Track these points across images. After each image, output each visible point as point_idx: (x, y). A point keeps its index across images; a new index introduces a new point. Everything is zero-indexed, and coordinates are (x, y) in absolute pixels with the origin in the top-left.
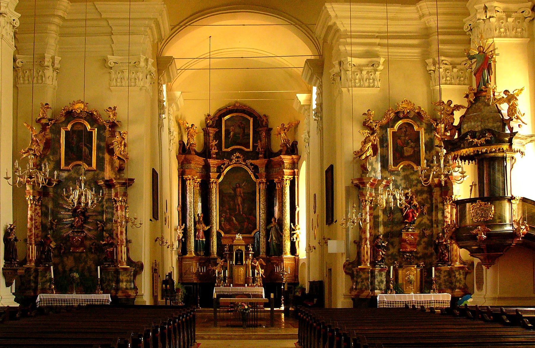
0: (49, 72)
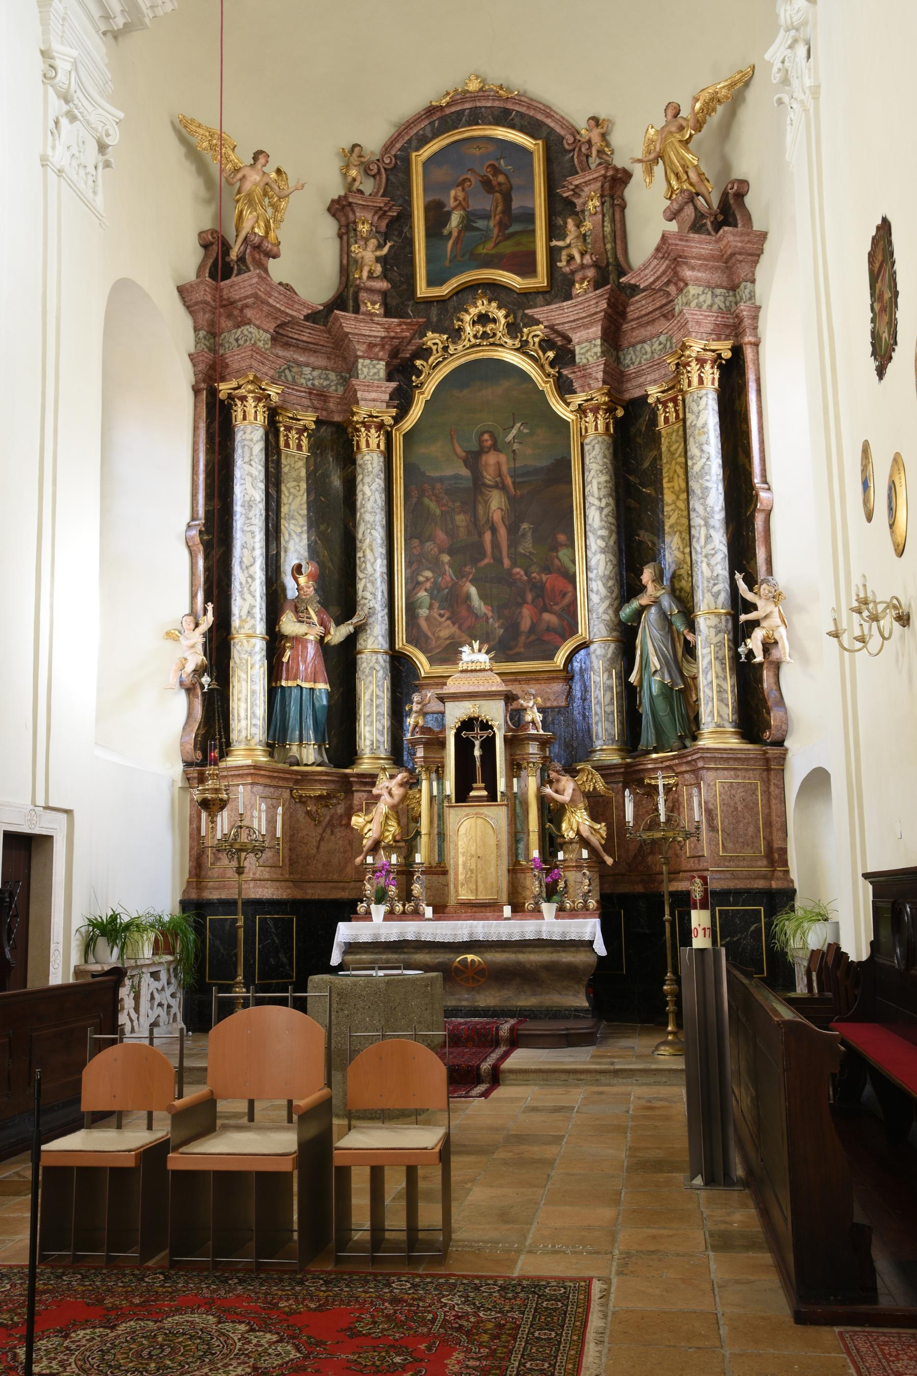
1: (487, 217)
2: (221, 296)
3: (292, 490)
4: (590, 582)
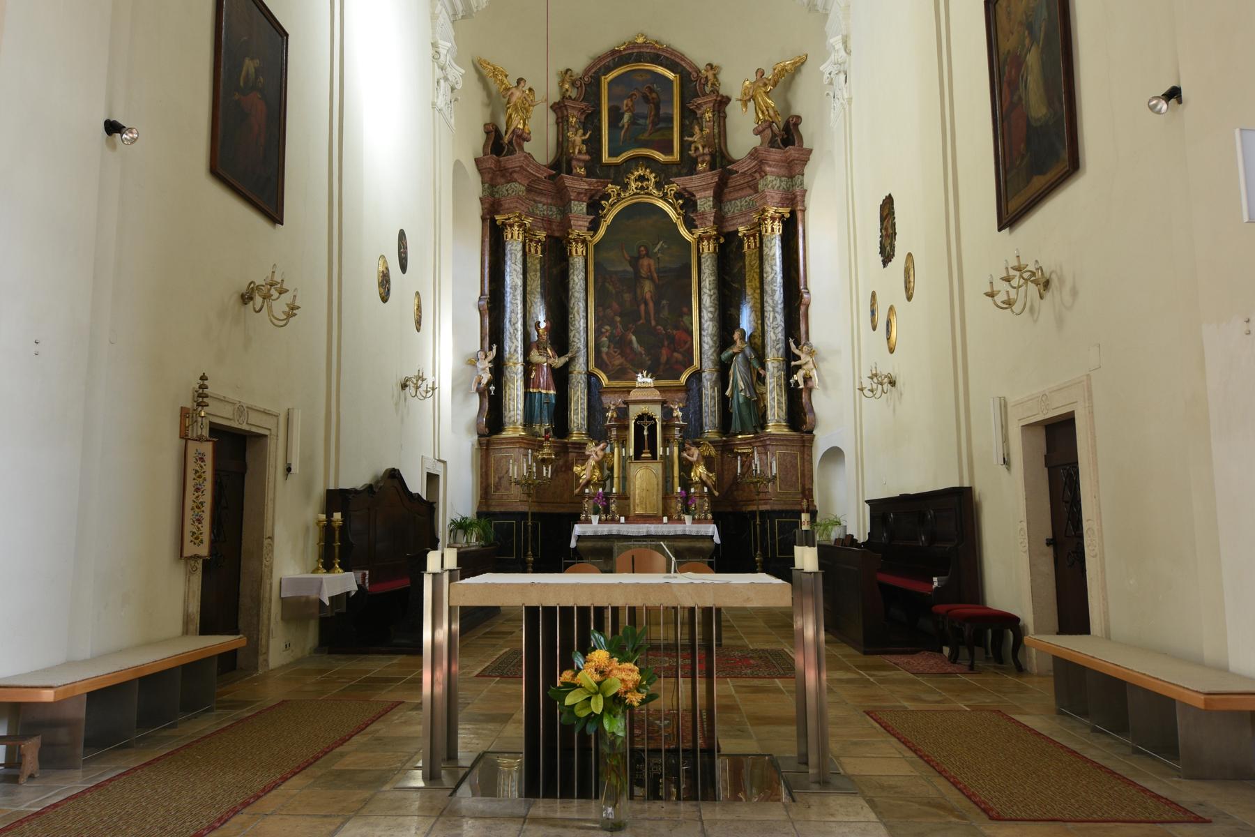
2: (500, 165)
3: (533, 277)
4: (703, 337)
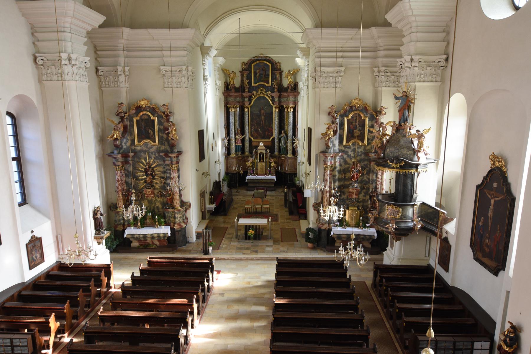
0: (122, 79)
1: (263, 74)
